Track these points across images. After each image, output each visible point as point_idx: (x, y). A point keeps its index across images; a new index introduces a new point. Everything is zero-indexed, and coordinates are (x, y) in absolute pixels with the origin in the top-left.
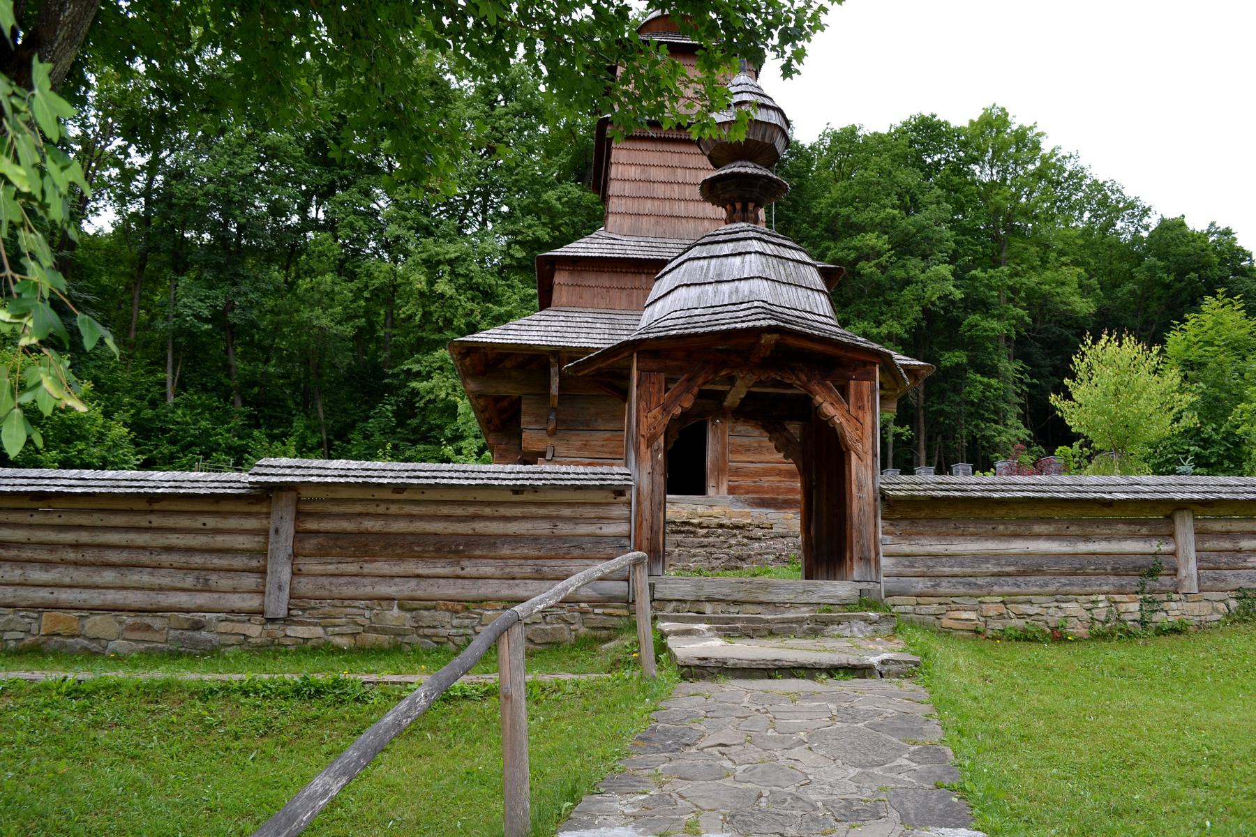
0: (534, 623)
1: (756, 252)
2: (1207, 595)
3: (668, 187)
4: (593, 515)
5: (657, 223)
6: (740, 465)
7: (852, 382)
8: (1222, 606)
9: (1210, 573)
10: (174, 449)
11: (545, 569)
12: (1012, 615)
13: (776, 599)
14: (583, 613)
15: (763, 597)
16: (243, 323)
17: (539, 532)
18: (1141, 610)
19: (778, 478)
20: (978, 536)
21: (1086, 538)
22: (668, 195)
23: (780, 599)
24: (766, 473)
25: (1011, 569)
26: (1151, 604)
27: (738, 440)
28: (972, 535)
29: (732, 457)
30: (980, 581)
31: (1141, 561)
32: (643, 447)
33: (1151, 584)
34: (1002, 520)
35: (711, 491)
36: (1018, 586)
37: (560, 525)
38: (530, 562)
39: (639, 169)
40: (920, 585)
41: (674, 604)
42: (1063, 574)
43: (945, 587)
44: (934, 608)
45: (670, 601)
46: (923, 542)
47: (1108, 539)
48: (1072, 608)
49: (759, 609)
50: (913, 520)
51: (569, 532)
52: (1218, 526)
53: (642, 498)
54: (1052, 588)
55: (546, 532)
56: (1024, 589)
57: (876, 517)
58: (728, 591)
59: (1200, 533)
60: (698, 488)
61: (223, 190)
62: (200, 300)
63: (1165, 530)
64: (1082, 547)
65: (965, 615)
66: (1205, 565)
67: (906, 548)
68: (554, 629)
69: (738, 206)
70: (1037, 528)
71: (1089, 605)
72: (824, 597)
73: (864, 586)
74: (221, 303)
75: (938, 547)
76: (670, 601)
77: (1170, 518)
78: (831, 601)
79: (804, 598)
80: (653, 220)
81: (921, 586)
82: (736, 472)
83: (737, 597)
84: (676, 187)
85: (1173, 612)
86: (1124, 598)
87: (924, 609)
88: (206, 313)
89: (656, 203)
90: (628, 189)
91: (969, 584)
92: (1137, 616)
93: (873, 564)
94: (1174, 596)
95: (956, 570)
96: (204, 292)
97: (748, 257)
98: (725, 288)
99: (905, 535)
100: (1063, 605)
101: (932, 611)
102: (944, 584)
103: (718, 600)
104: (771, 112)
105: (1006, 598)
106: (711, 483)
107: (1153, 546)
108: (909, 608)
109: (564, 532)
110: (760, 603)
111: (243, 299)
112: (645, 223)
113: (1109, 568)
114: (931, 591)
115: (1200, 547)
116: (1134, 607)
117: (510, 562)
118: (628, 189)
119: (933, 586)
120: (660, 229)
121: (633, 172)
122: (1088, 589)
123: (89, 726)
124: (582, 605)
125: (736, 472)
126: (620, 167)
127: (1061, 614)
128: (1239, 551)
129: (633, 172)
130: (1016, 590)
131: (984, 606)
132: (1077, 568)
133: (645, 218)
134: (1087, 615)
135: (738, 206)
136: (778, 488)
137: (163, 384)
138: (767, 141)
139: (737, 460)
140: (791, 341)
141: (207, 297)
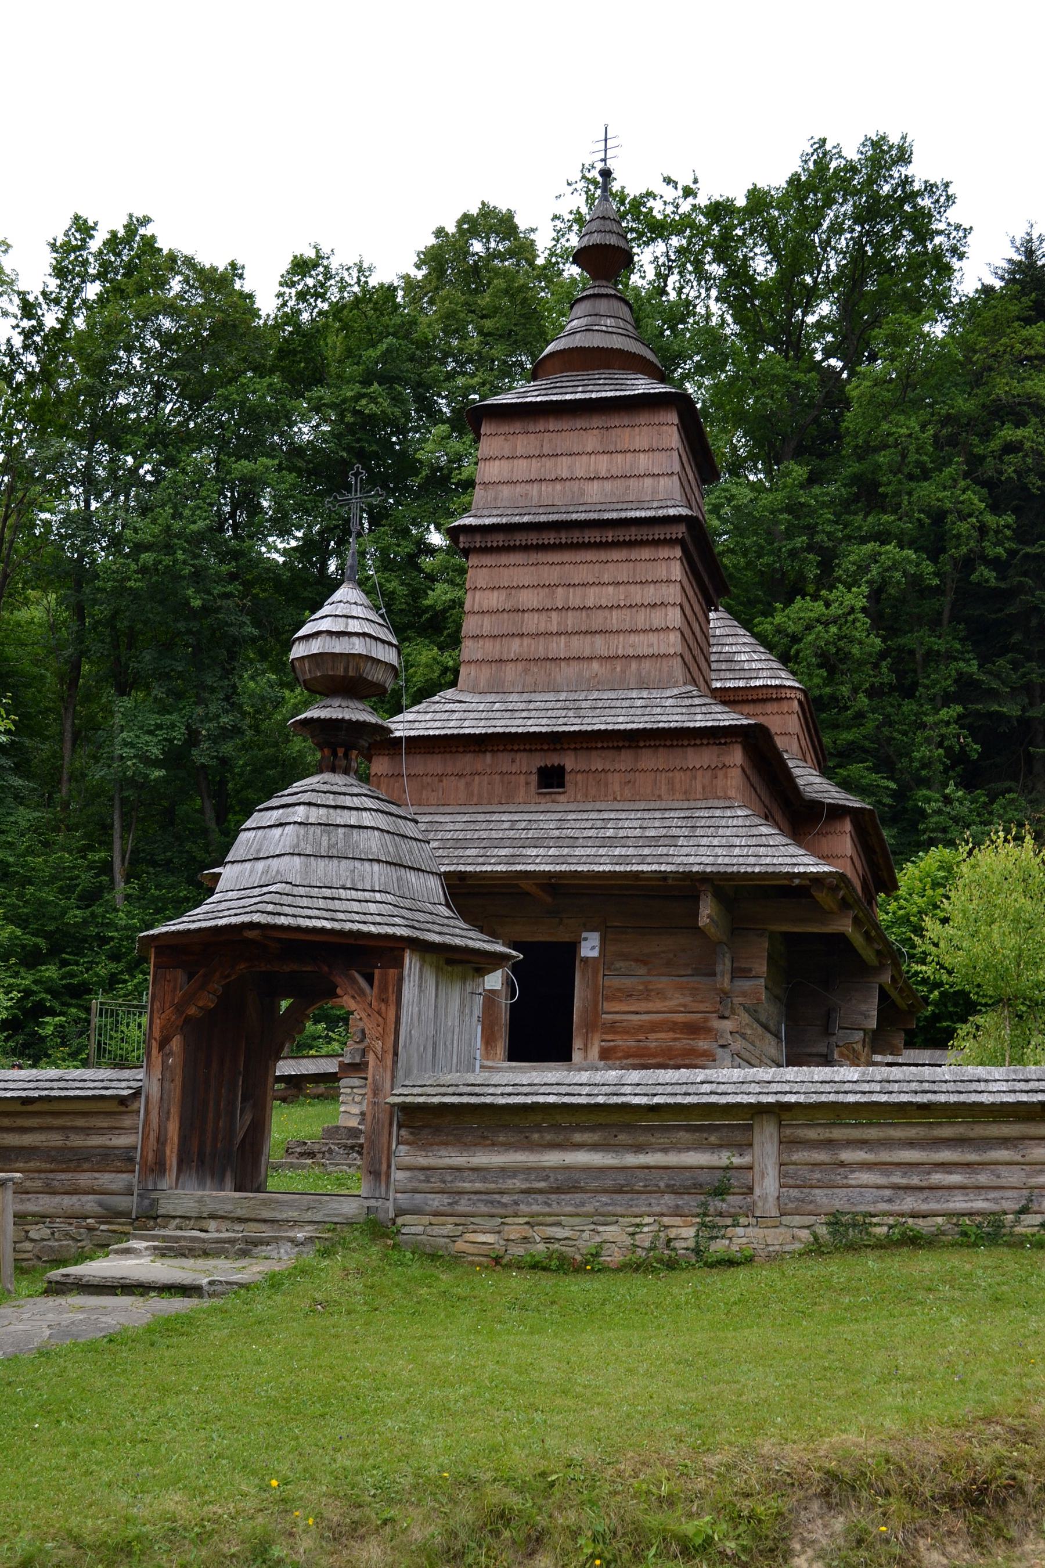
0: (43, 1240)
1: (295, 823)
2: (786, 1220)
3: (544, 616)
5: (526, 671)
6: (618, 1017)
7: (377, 971)
8: (805, 1234)
9: (794, 1193)
10: (113, 967)
11: (56, 1183)
12: (538, 1239)
13: (279, 1216)
14: (90, 1229)
15: (266, 1214)
16: (215, 762)
17: (52, 1144)
18: (697, 1236)
19: (671, 1035)
20: (508, 1146)
21: (639, 1148)
22: (542, 629)
23: (284, 1216)
24: (654, 1027)
25: (542, 1185)
26: (710, 1229)
27: (616, 982)
28: (503, 1144)
29: (607, 1006)
30: (505, 1199)
31: (704, 1177)
32: (155, 1051)
33: (717, 1204)
34: (538, 1128)
35: (577, 1056)
36: (549, 1205)
37: (72, 1137)
38: (43, 1175)
40: (437, 1202)
41: (178, 1220)
42: (605, 1191)
43: (463, 1206)
44: (448, 1229)
45: (174, 1217)
46: (443, 1153)
47: (665, 1150)
48: (610, 1232)
49: (263, 1227)
50: (437, 1130)
51: (81, 1143)
52: (812, 1134)
53: (150, 1107)
54: (589, 1208)
55: (59, 1143)
56: (555, 1208)
57: (391, 1125)
58: (229, 1207)
59: (788, 1143)
61: (167, 560)
62: (150, 733)
64: (632, 1159)
65: (482, 1238)
66: (791, 1182)
67: (423, 1161)
68: (61, 1246)
69: (341, 752)
70: (578, 1137)
71: (631, 1229)
72: (329, 1215)
73: (372, 1203)
74: (179, 735)
75: (458, 1159)
76: (174, 1217)
78: (336, 1220)
79: (309, 1216)
80: (520, 666)
81: (436, 1203)
82: (612, 1028)
83: (239, 1213)
84: (554, 615)
85: (742, 1237)
86: (677, 1221)
87: (436, 1230)
88: (156, 752)
89: (526, 641)
90: (488, 624)
91: (492, 1202)
92: (691, 1243)
93: (383, 1178)
94: (743, 1220)
95: (479, 1186)
96: (153, 719)
97: (287, 828)
98: (260, 865)
99: (425, 1147)
100: (601, 1229)
101: (445, 1232)
102: (463, 1202)
103: (222, 1217)
104: (355, 640)
105: (531, 1220)
106: (577, 1043)
107: (723, 1158)
108: (420, 1229)
109: (76, 1144)
110: (265, 1221)
111: (212, 725)
112: (510, 672)
113: (662, 1184)
114: (447, 1209)
115: (785, 1158)
116: (690, 1232)
118: (488, 624)
119: (450, 1204)
120: (529, 679)
121: (494, 600)
122: (635, 1210)
123: (943, 1535)
124: (89, 1221)
125: (612, 1028)
126: (478, 594)
127: (598, 1239)
128: (842, 1164)
129: (494, 600)
130: (547, 1210)
131: (506, 1228)
132: (623, 1185)
133: (510, 665)
134: (629, 1241)
135: (341, 752)
136: (670, 1049)
137: (106, 868)
138: (351, 674)
139: (614, 1011)
141: (159, 727)
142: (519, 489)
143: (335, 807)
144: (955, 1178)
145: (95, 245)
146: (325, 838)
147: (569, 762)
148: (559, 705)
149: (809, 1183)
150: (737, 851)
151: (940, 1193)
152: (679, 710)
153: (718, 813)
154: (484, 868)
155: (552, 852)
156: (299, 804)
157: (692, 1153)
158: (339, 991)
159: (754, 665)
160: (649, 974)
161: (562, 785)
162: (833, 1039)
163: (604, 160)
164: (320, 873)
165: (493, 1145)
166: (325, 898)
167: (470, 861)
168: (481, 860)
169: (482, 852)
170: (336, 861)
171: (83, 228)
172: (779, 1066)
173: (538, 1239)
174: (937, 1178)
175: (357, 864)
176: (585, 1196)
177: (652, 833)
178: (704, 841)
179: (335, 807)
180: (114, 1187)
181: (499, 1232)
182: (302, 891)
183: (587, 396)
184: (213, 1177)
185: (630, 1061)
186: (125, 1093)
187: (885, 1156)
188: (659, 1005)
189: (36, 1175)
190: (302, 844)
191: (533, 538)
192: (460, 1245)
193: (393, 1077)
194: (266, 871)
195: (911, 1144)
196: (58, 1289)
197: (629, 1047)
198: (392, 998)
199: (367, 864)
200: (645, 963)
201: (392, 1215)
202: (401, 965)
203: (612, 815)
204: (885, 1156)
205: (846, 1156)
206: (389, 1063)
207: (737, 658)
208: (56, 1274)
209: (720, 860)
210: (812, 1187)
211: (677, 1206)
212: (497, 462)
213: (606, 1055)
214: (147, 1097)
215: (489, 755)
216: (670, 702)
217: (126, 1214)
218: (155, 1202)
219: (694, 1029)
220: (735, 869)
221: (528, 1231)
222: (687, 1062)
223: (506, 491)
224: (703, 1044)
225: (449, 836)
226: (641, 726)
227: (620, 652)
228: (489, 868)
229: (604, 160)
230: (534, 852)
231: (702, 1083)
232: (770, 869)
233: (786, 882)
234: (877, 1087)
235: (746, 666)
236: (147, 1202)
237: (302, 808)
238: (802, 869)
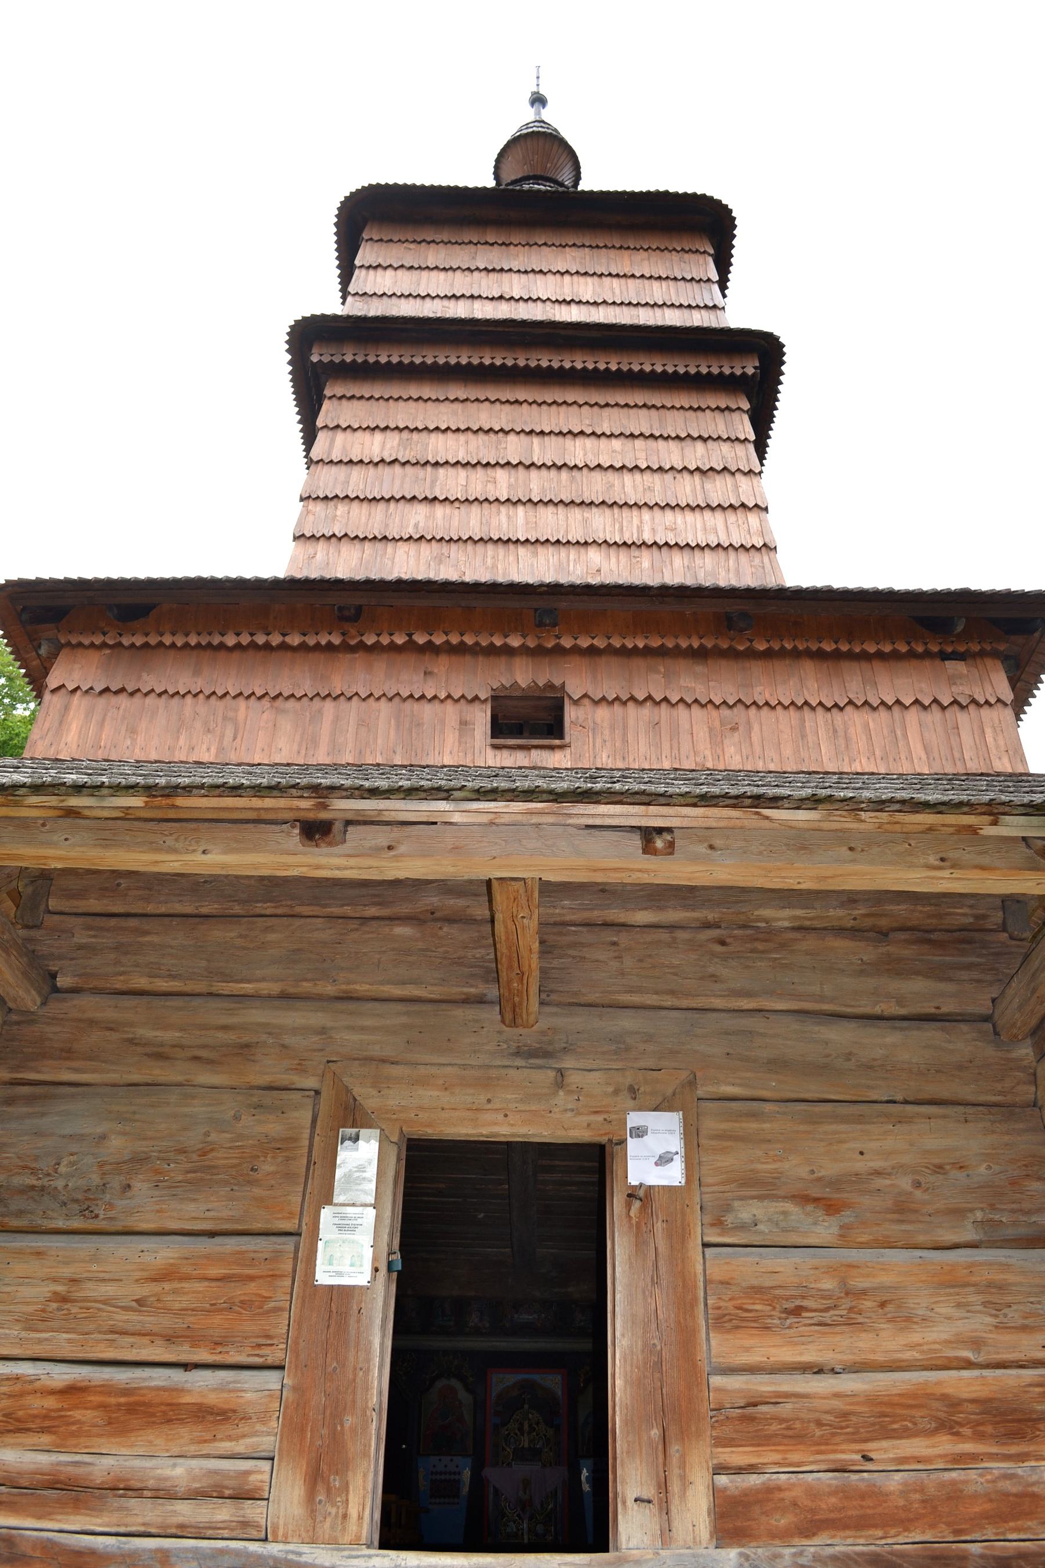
106: (631, 1479)
188: (890, 1342)
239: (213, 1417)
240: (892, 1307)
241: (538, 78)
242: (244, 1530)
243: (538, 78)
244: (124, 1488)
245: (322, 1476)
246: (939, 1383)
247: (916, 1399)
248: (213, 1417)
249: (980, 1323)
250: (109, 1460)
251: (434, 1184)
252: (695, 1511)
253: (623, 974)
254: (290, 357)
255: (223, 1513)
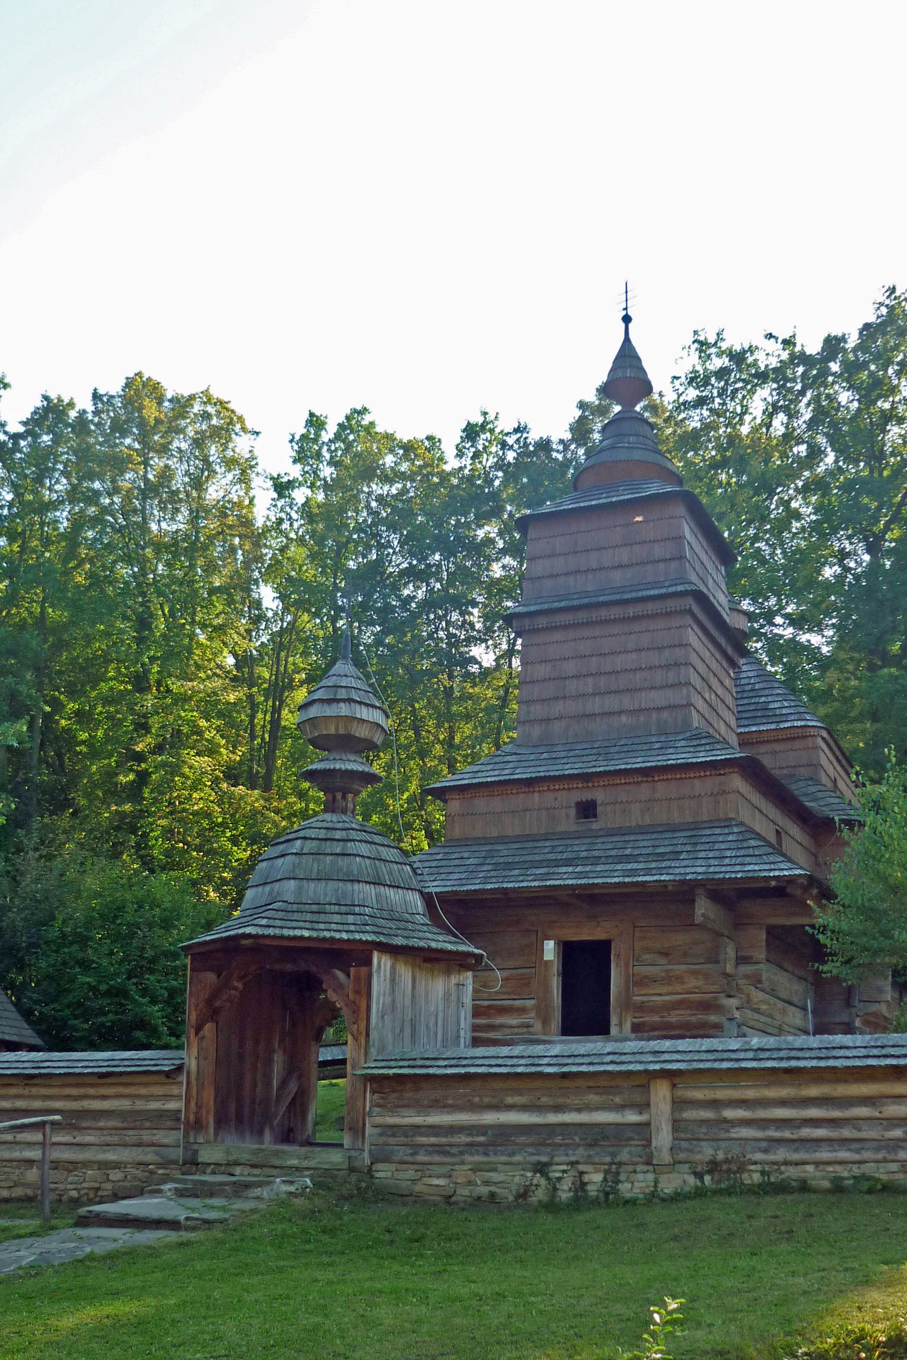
4: (161, 1093)
6: (645, 998)
12: (479, 1183)
15: (277, 1162)
21: (558, 1108)
25: (482, 1139)
28: (451, 1106)
35: (614, 1030)
38: (118, 1132)
39: (549, 666)
43: (421, 1158)
44: (411, 1174)
45: (209, 1164)
47: (579, 1110)
56: (492, 1159)
60: (600, 1027)
63: (638, 1098)
65: (436, 1182)
69: (339, 795)
77: (645, 1088)
79: (305, 1164)
82: (641, 1008)
87: (401, 1175)
104: (342, 705)
106: (614, 1020)
114: (410, 1159)
115: (677, 1116)
117: (105, 1132)
119: (411, 1154)
128: (725, 1121)
135: (339, 795)
140: (262, 941)
142: (562, 580)
143: (326, 840)
144: (821, 1133)
145: (327, 436)
146: (315, 865)
147: (599, 796)
148: (594, 751)
149: (696, 1136)
150: (727, 861)
151: (808, 1145)
152: (688, 749)
153: (718, 831)
154: (522, 885)
155: (579, 869)
156: (297, 839)
157: (600, 1112)
158: (324, 986)
159: (784, 711)
160: (669, 964)
161: (595, 816)
162: (853, 1010)
163: (626, 309)
164: (311, 893)
165: (444, 1107)
166: (312, 912)
167: (512, 879)
168: (521, 878)
169: (523, 871)
170: (324, 882)
171: (315, 422)
172: (807, 1033)
173: (479, 1183)
174: (806, 1132)
175: (341, 884)
176: (516, 1148)
177: (661, 850)
178: (702, 855)
179: (326, 840)
180: (166, 1141)
181: (450, 1177)
182: (295, 907)
183: (608, 500)
184: (252, 1132)
185: (656, 1033)
186: (167, 1069)
187: (761, 1114)
188: (678, 988)
189: (113, 1132)
190: (297, 871)
191: (568, 618)
192: (418, 1188)
193: (366, 1054)
194: (270, 893)
195: (783, 1103)
196: (83, 1222)
197: (655, 1022)
198: (364, 990)
199: (349, 884)
200: (666, 954)
201: (368, 1161)
202: (369, 963)
203: (632, 838)
204: (761, 1114)
205: (729, 1113)
206: (363, 1042)
207: (772, 706)
208: (83, 1211)
209: (711, 869)
210: (699, 1140)
211: (589, 1156)
212: (541, 560)
213: (637, 1028)
214: (188, 1073)
215: (536, 795)
216: (683, 743)
217: (175, 1162)
218: (196, 1152)
219: (707, 1006)
220: (721, 876)
221: (472, 1177)
222: (701, 1032)
223: (548, 583)
224: (713, 1018)
225: (502, 860)
226: (653, 764)
227: (643, 706)
228: (525, 884)
229: (626, 309)
230: (564, 869)
231: (609, 1054)
232: (750, 875)
233: (763, 885)
234: (651, 1058)
235: (778, 712)
236: (190, 1153)
237: (299, 842)
238: (777, 873)
239: (522, 1010)
240: (679, 979)
241: (627, 319)
242: (529, 1033)
243: (627, 319)
244: (502, 1026)
245: (545, 1022)
246: (794, 914)
247: (681, 1002)
248: (522, 1010)
249: (701, 983)
250: (498, 1021)
251: (568, 950)
252: (628, 1026)
253: (389, 1231)
254: (553, 423)
255: (525, 1030)
